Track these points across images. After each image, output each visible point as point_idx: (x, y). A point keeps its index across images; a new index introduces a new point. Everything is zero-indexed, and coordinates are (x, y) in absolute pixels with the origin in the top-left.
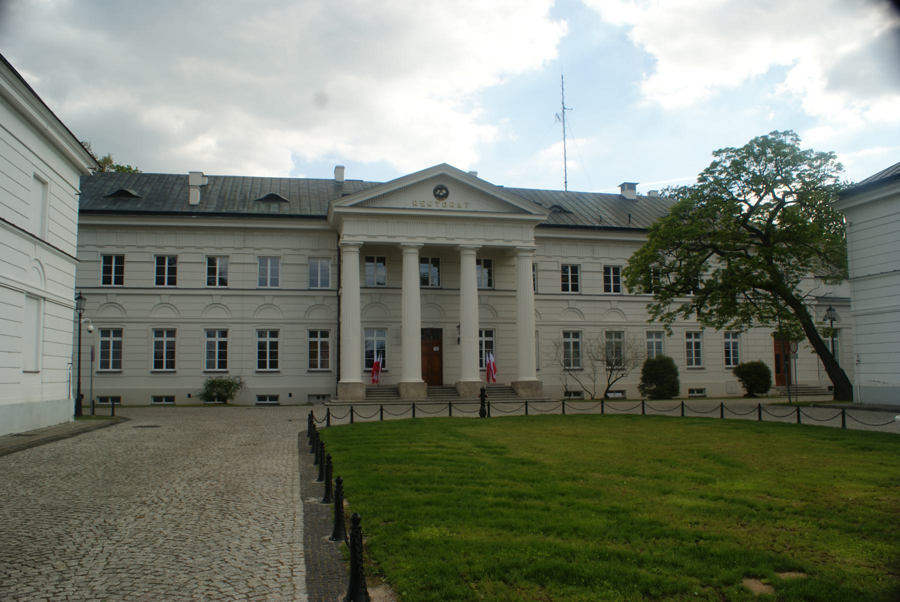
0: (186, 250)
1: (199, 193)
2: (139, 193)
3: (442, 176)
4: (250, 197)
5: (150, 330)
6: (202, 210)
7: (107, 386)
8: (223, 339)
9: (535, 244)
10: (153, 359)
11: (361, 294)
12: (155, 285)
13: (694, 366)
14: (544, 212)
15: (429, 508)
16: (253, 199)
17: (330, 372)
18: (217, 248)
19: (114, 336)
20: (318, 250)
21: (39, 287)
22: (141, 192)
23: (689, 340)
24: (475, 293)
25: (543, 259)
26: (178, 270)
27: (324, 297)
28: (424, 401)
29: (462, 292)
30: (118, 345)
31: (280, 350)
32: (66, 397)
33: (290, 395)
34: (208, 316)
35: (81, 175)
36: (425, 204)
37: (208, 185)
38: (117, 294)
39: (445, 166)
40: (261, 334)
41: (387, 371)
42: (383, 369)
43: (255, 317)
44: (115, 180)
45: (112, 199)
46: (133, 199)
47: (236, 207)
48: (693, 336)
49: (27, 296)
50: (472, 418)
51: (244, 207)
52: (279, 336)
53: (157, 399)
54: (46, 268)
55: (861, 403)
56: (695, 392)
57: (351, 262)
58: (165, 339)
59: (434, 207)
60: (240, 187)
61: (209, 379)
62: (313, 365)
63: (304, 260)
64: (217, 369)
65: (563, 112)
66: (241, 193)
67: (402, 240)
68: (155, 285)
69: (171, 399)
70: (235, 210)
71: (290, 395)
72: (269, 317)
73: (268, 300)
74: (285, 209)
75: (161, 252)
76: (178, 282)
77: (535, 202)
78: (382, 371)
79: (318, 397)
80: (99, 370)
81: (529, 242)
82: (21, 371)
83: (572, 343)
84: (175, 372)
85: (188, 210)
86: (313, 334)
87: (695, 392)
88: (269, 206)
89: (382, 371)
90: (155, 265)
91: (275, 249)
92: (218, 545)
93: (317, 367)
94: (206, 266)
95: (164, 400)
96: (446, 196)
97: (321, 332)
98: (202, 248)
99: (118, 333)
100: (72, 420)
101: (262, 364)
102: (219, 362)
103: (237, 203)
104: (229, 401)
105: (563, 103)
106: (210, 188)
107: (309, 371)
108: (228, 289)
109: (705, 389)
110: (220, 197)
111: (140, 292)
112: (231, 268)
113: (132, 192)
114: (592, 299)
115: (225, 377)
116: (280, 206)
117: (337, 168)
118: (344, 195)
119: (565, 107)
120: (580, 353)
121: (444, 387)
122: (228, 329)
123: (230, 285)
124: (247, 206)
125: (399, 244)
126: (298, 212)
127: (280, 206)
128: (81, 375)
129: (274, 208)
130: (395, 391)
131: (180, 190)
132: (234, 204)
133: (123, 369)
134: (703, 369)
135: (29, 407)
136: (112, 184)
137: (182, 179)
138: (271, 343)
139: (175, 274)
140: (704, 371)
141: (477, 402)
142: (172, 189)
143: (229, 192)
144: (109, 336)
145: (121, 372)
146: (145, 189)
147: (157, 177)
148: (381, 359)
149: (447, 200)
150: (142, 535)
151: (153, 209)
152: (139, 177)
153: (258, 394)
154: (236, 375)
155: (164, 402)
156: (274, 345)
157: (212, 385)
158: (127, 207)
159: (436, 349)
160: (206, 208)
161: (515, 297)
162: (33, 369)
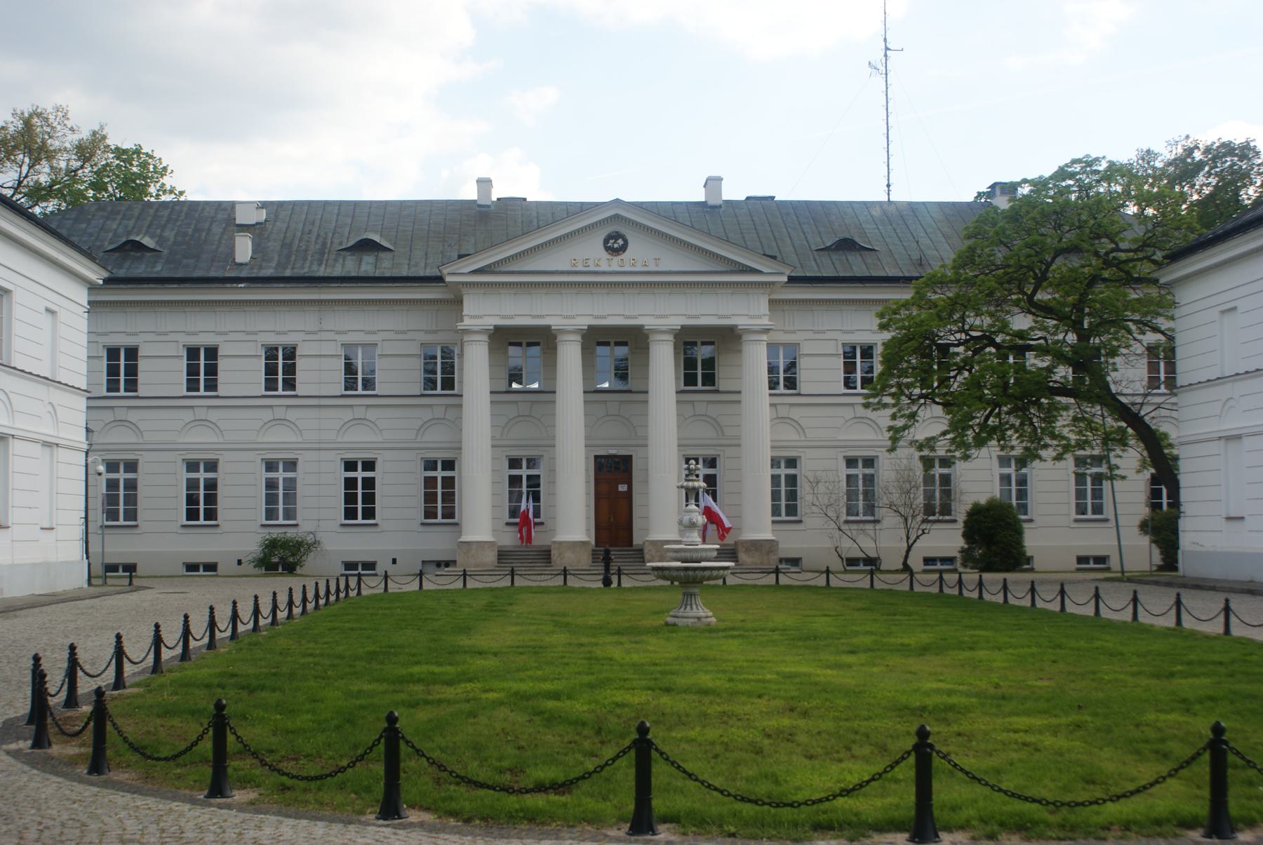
0: (232, 336)
2: (157, 243)
4: (332, 243)
7: (121, 547)
9: (770, 320)
10: (185, 507)
13: (1090, 516)
15: (739, 806)
17: (1106, 520)
18: (278, 333)
20: (435, 332)
21: (52, 433)
22: (161, 240)
25: (810, 335)
26: (220, 368)
27: (447, 406)
28: (589, 570)
30: (131, 485)
32: (79, 558)
33: (394, 561)
34: (266, 439)
35: (89, 286)
37: (266, 221)
39: (617, 201)
40: (350, 465)
41: (542, 524)
42: (537, 520)
43: (339, 440)
44: (120, 217)
45: (117, 255)
46: (148, 254)
47: (307, 264)
49: (43, 445)
50: (554, 587)
53: (192, 567)
54: (59, 409)
55: (1184, 577)
56: (1091, 562)
59: (604, 267)
60: (317, 223)
61: (267, 537)
63: (414, 349)
65: (886, 55)
66: (318, 236)
69: (211, 567)
70: (304, 271)
71: (394, 561)
72: (360, 441)
73: (359, 413)
74: (386, 266)
75: (273, 340)
77: (764, 255)
78: (536, 524)
79: (439, 564)
81: (759, 317)
82: (38, 527)
85: (233, 274)
87: (1091, 562)
89: (536, 524)
93: (436, 518)
95: (201, 569)
96: (623, 248)
97: (443, 462)
98: (255, 333)
99: (132, 466)
100: (86, 586)
101: (350, 513)
103: (309, 258)
104: (299, 570)
105: (885, 40)
106: (269, 226)
107: (423, 524)
108: (296, 396)
109: (1108, 556)
110: (283, 245)
111: (163, 402)
113: (148, 241)
115: (291, 533)
117: (479, 181)
118: (460, 257)
119: (889, 46)
120: (953, 493)
121: (634, 548)
122: (297, 459)
124: (324, 262)
126: (404, 272)
127: (377, 258)
128: (1120, 524)
129: (367, 265)
130: (545, 555)
131: (223, 234)
132: (305, 259)
133: (139, 522)
135: (47, 566)
137: (225, 210)
140: (218, 530)
141: (600, 572)
142: (209, 230)
143: (299, 234)
144: (118, 472)
145: (136, 526)
146: (166, 234)
147: (185, 209)
149: (626, 256)
152: (157, 210)
154: (309, 530)
155: (201, 572)
158: (140, 270)
159: (623, 488)
160: (261, 268)
162: (47, 526)
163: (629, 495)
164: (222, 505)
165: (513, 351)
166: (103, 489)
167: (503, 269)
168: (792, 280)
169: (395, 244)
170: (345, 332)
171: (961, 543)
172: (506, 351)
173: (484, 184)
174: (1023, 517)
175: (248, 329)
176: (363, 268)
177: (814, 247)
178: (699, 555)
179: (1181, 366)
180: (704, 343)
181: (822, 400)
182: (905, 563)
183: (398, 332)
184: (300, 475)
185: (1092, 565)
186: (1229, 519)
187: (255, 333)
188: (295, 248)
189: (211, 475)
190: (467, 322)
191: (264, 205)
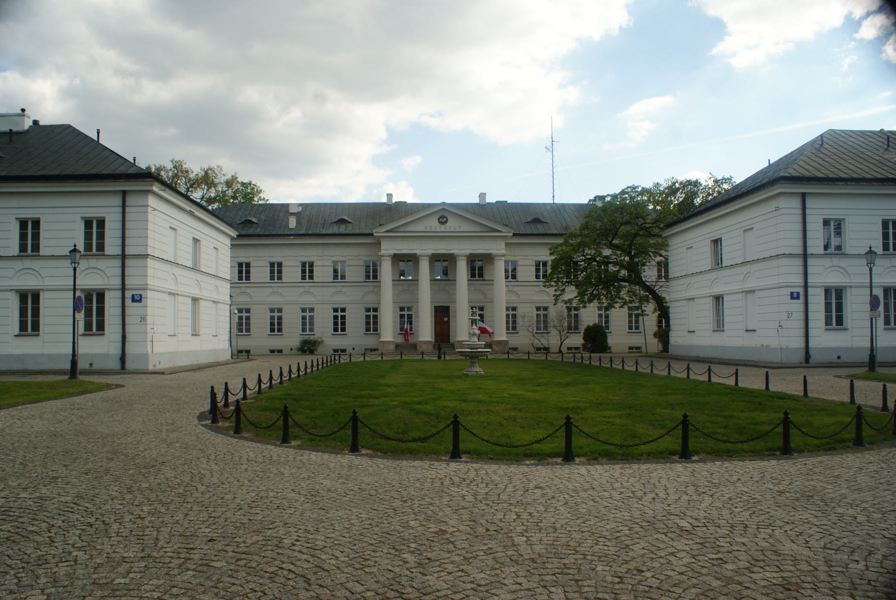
1: (295, 220)
2: (258, 220)
3: (443, 209)
5: (534, 307)
6: (297, 232)
11: (393, 285)
14: (510, 230)
16: (330, 222)
20: (369, 256)
22: (259, 219)
24: (391, 283)
26: (314, 271)
29: (420, 282)
30: (248, 318)
33: (353, 349)
34: (302, 299)
36: (433, 228)
38: (247, 287)
39: (444, 203)
40: (336, 310)
41: (413, 334)
44: (243, 210)
46: (254, 225)
48: (244, 312)
51: (323, 229)
52: (346, 311)
53: (272, 351)
59: (438, 230)
62: (368, 329)
63: (362, 263)
64: (308, 333)
67: (455, 252)
68: (238, 281)
69: (280, 351)
70: (317, 232)
71: (353, 349)
72: (339, 300)
74: (350, 230)
75: (272, 260)
76: (283, 278)
78: (410, 334)
79: (371, 350)
81: (501, 250)
83: (276, 317)
84: (282, 335)
86: (368, 310)
88: (340, 227)
90: (269, 268)
91: (343, 256)
94: (237, 269)
96: (446, 222)
101: (336, 330)
102: (246, 329)
107: (365, 334)
108: (314, 282)
112: (347, 269)
113: (254, 220)
114: (292, 285)
115: (312, 337)
116: (346, 227)
126: (357, 232)
127: (346, 227)
129: (342, 229)
133: (283, 333)
136: (241, 214)
138: (341, 316)
139: (313, 273)
140: (283, 337)
148: (409, 326)
149: (447, 225)
150: (123, 446)
151: (267, 233)
153: (334, 348)
155: (276, 353)
157: (304, 343)
158: (251, 231)
159: (446, 319)
161: (493, 284)
162: (173, 334)
165: (401, 263)
168: (514, 235)
171: (582, 341)
174: (607, 331)
180: (478, 261)
182: (560, 350)
183: (354, 256)
186: (689, 332)
190: (383, 252)
191: (300, 205)
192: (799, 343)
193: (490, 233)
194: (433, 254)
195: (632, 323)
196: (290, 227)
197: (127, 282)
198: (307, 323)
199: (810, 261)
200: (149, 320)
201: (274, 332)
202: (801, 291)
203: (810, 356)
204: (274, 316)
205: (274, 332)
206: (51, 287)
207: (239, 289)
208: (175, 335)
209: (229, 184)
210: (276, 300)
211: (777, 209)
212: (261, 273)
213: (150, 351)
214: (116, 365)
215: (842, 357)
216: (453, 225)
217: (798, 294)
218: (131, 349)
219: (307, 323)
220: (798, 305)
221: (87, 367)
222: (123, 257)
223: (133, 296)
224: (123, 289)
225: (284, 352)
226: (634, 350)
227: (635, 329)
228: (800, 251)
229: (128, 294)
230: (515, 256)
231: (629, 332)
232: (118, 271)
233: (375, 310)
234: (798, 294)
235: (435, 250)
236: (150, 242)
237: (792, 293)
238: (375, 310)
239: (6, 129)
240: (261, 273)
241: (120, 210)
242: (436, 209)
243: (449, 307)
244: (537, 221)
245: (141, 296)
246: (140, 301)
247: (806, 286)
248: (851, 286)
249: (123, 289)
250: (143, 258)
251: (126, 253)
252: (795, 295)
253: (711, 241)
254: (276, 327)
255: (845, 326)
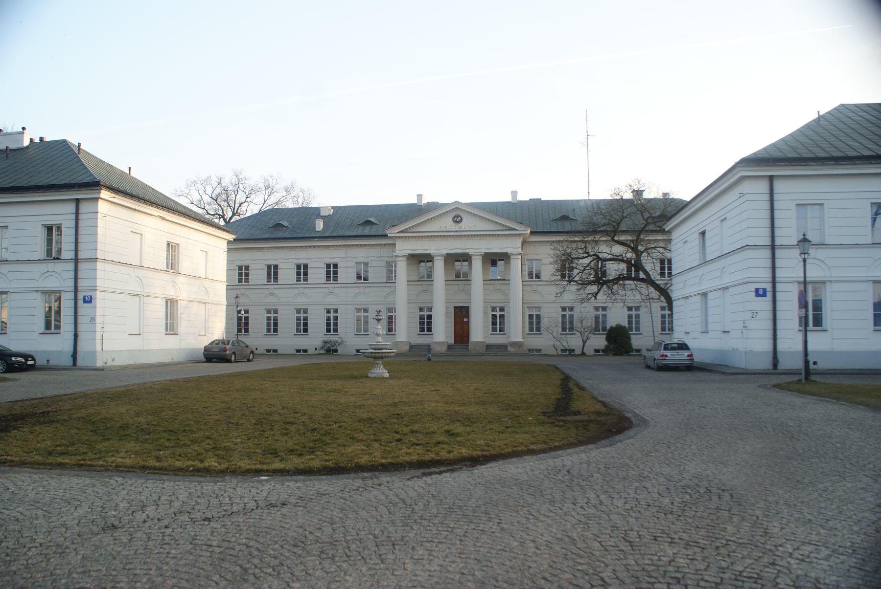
2: (289, 224)
3: (457, 209)
8: (430, 313)
12: (237, 283)
18: (331, 258)
19: (602, 311)
23: (663, 312)
24: (406, 283)
26: (250, 274)
31: (250, 321)
39: (457, 202)
48: (272, 312)
57: (402, 267)
58: (568, 313)
63: (384, 264)
68: (237, 283)
75: (299, 262)
80: (266, 333)
83: (601, 316)
92: (103, 436)
96: (461, 221)
98: (322, 259)
102: (274, 329)
107: (418, 334)
113: (285, 223)
123: (543, 278)
125: (468, 253)
129: (367, 231)
134: (641, 334)
149: (461, 224)
156: (336, 318)
159: (466, 320)
163: (468, 323)
164: (250, 327)
165: (457, 263)
166: (660, 320)
167: (411, 231)
168: (532, 233)
169: (379, 222)
170: (266, 260)
171: (605, 343)
172: (454, 263)
173: (514, 193)
174: (630, 332)
175: (308, 257)
176: (365, 232)
177: (551, 219)
178: (381, 347)
179: (674, 267)
180: (499, 260)
181: (258, 287)
182: (582, 352)
183: (377, 257)
184: (608, 313)
185: (535, 353)
186: (724, 332)
187: (322, 259)
188: (340, 224)
189: (305, 315)
190: (397, 253)
191: (333, 208)
192: (768, 346)
193: (507, 233)
194: (447, 254)
195: (632, 324)
196: (317, 230)
197: (79, 285)
198: (332, 325)
199: (779, 253)
200: (98, 319)
201: (330, 332)
202: (769, 287)
203: (778, 361)
204: (424, 315)
205: (330, 332)
206: (116, 290)
207: (297, 290)
208: (140, 334)
209: (288, 190)
210: (302, 301)
211: (742, 195)
212: (258, 275)
213: (99, 348)
214: (68, 361)
215: (818, 363)
216: (468, 224)
217: (765, 290)
218: (82, 347)
219: (332, 325)
220: (765, 303)
221: (45, 363)
222: (76, 260)
223: (84, 297)
224: (76, 291)
225: (309, 352)
226: (302, 353)
227: (274, 332)
228: (767, 241)
229: (81, 296)
230: (539, 255)
231: (661, 334)
232: (72, 275)
233: (502, 309)
234: (765, 290)
235: (488, 249)
236: (100, 246)
237: (757, 290)
238: (502, 309)
239: (3, 147)
240: (258, 275)
241: (74, 217)
242: (452, 208)
243: (469, 307)
244: (565, 218)
245: (91, 297)
246: (90, 302)
247: (774, 282)
248: (831, 281)
249: (76, 291)
250: (93, 261)
251: (79, 257)
252: (761, 292)
253: (700, 233)
254: (272, 327)
255: (824, 327)
